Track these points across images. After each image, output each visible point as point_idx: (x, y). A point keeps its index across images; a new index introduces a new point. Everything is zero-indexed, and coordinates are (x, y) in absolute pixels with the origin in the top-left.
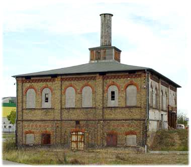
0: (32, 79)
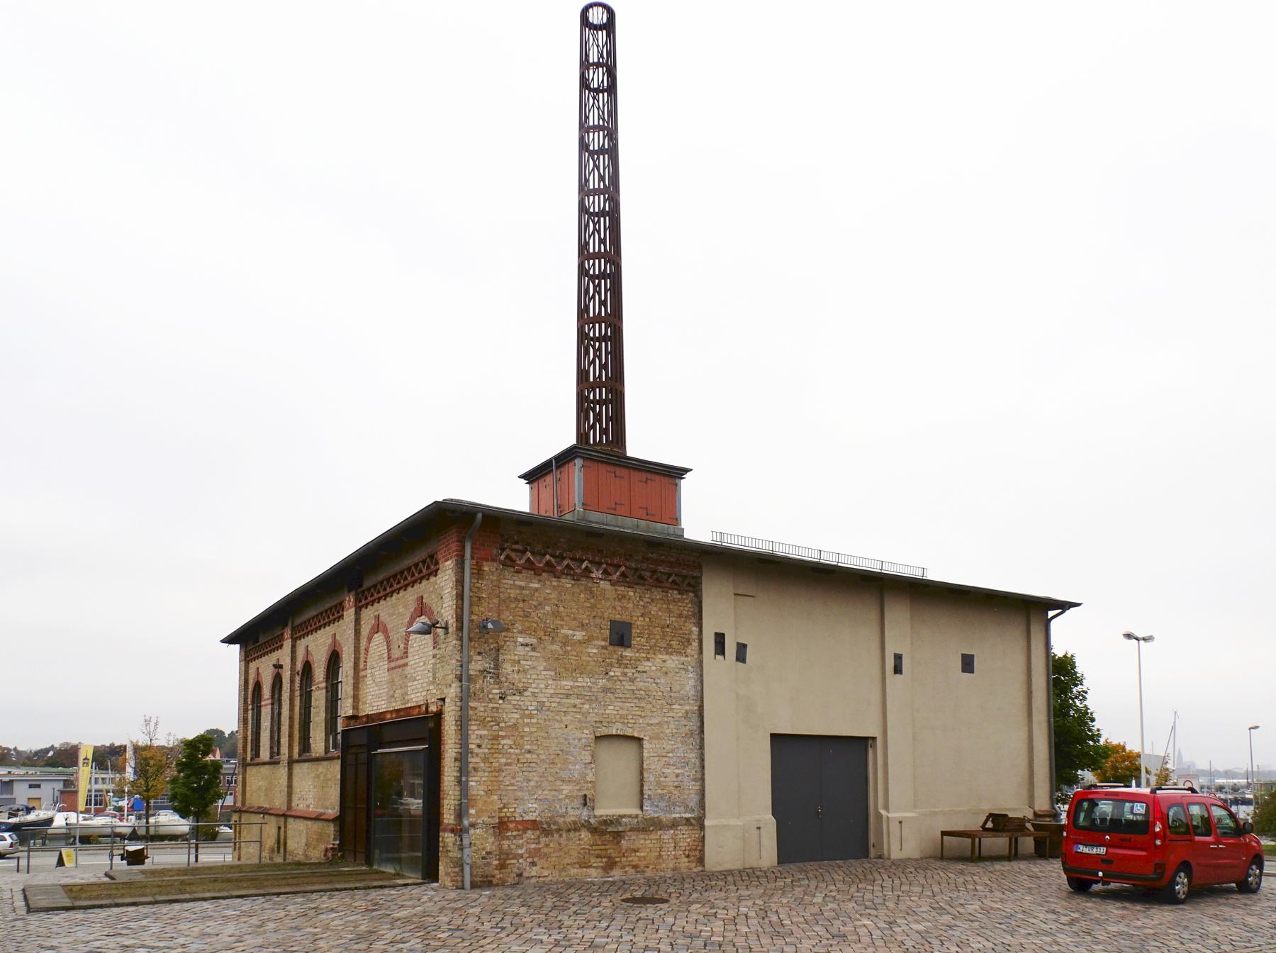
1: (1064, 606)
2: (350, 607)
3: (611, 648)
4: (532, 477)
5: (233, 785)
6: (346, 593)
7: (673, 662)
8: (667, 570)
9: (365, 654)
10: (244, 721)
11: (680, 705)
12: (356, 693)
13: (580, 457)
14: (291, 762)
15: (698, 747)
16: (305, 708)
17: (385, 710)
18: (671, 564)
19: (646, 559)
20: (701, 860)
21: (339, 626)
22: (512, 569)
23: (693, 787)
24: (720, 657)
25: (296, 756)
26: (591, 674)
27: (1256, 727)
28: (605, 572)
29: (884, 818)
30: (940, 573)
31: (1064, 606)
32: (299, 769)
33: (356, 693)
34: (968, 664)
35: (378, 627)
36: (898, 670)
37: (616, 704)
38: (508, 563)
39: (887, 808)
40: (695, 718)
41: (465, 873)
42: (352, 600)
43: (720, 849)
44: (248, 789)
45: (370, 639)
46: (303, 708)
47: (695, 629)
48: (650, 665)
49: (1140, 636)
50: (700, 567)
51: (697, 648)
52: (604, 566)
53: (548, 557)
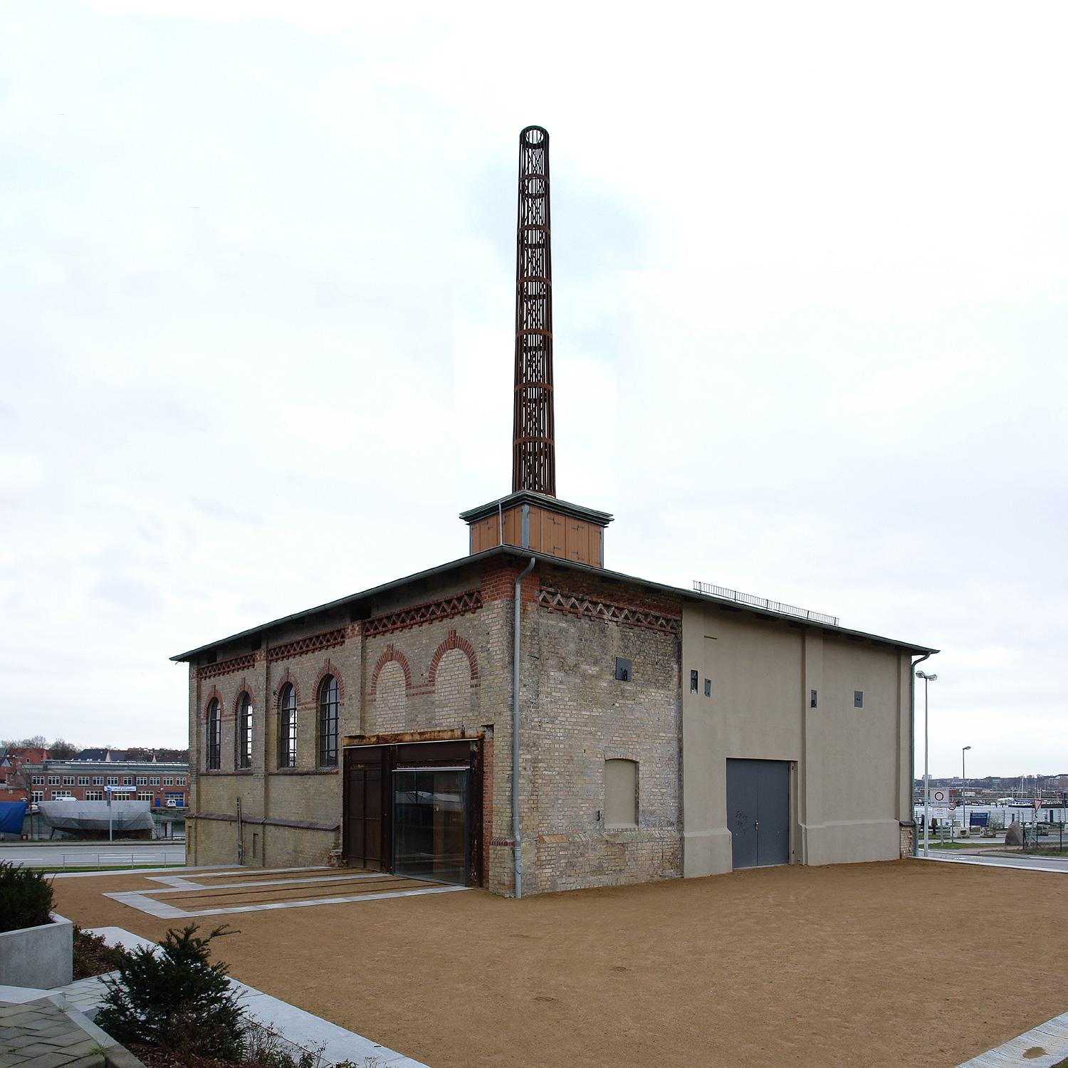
0: (220, 659)
1: (926, 652)
2: (354, 635)
3: (616, 681)
4: (473, 518)
5: (40, 784)
6: (348, 622)
7: (656, 694)
8: (657, 614)
9: (373, 679)
10: (194, 733)
11: (664, 732)
12: (680, 736)
13: (526, 503)
14: (268, 774)
15: (677, 770)
16: (282, 725)
17: (402, 732)
18: (661, 609)
19: (643, 604)
20: (680, 867)
21: (334, 652)
22: (546, 610)
23: (672, 804)
24: (694, 691)
25: (203, 768)
26: (603, 705)
27: (968, 748)
28: (614, 615)
29: (803, 830)
30: (850, 621)
31: (926, 652)
32: (274, 781)
33: (363, 715)
34: (858, 699)
35: (391, 655)
36: (814, 704)
37: (621, 732)
38: (545, 604)
39: (804, 821)
40: (674, 744)
41: (516, 882)
42: (357, 629)
43: (694, 858)
44: (203, 797)
45: (379, 666)
46: (280, 725)
47: (675, 666)
48: (644, 697)
49: (927, 675)
50: (681, 612)
51: (677, 683)
52: (613, 608)
53: (573, 599)
